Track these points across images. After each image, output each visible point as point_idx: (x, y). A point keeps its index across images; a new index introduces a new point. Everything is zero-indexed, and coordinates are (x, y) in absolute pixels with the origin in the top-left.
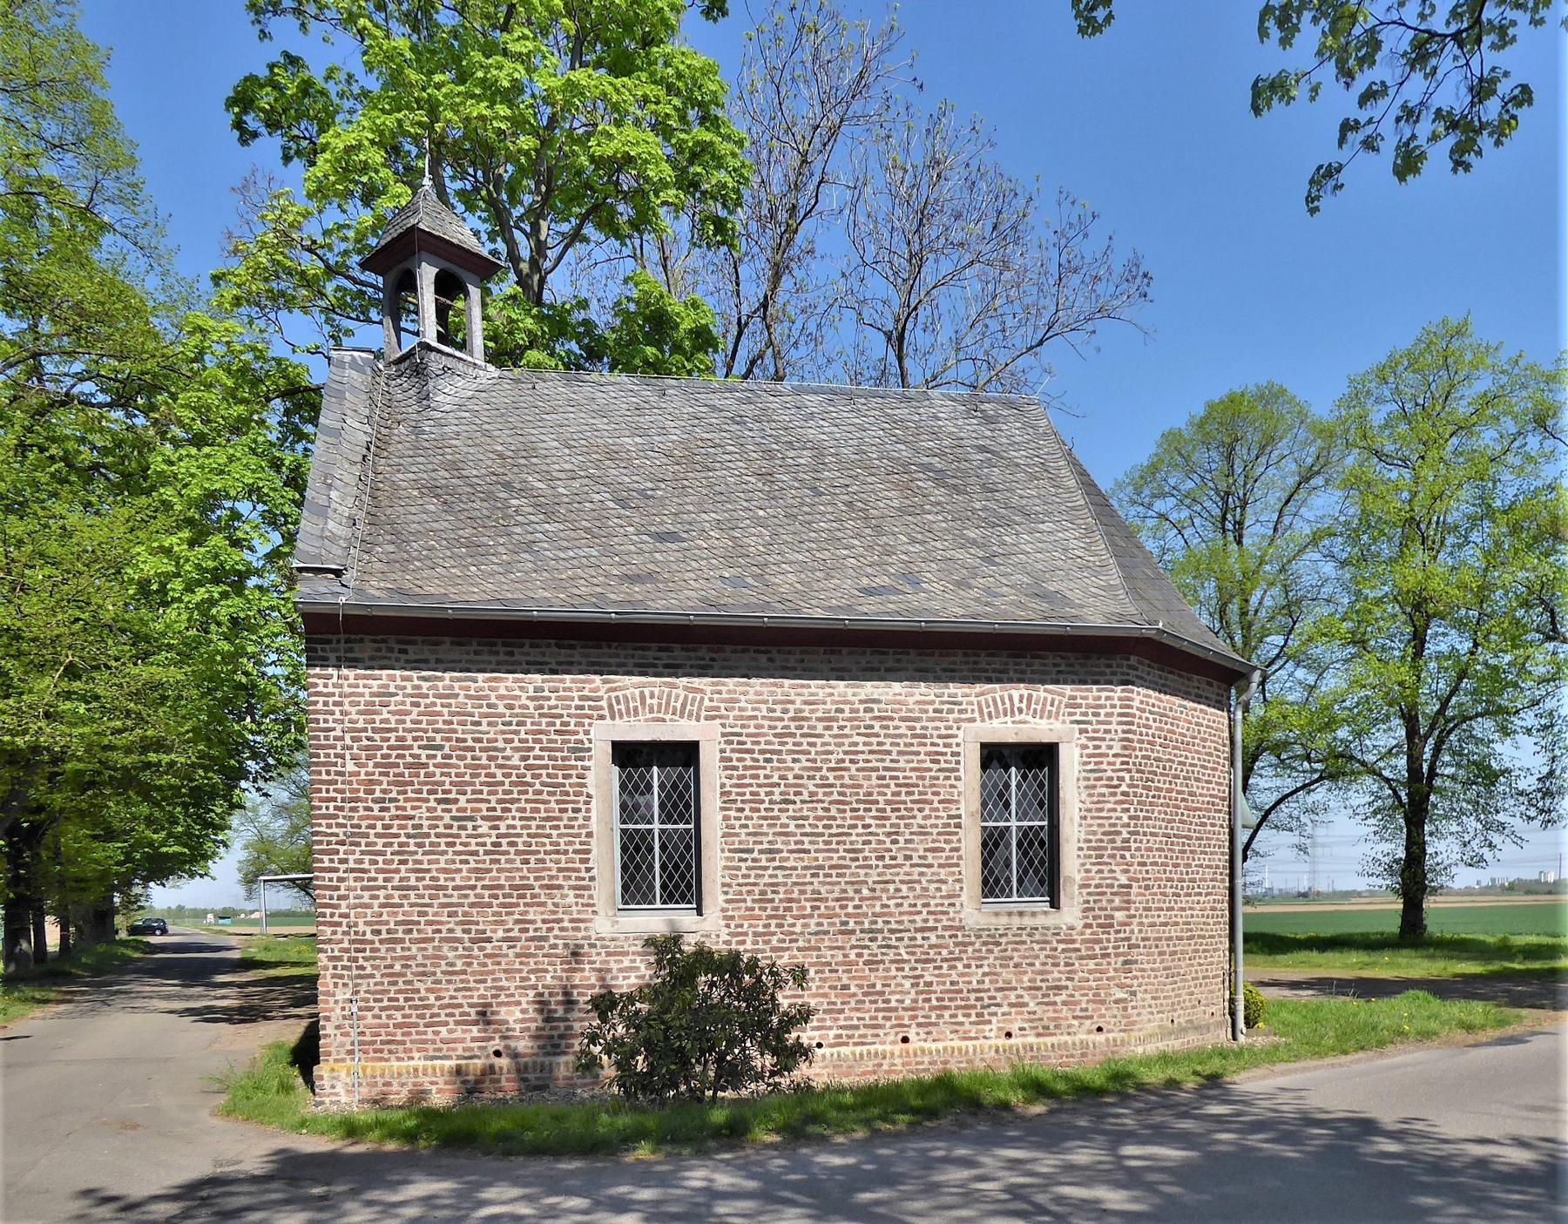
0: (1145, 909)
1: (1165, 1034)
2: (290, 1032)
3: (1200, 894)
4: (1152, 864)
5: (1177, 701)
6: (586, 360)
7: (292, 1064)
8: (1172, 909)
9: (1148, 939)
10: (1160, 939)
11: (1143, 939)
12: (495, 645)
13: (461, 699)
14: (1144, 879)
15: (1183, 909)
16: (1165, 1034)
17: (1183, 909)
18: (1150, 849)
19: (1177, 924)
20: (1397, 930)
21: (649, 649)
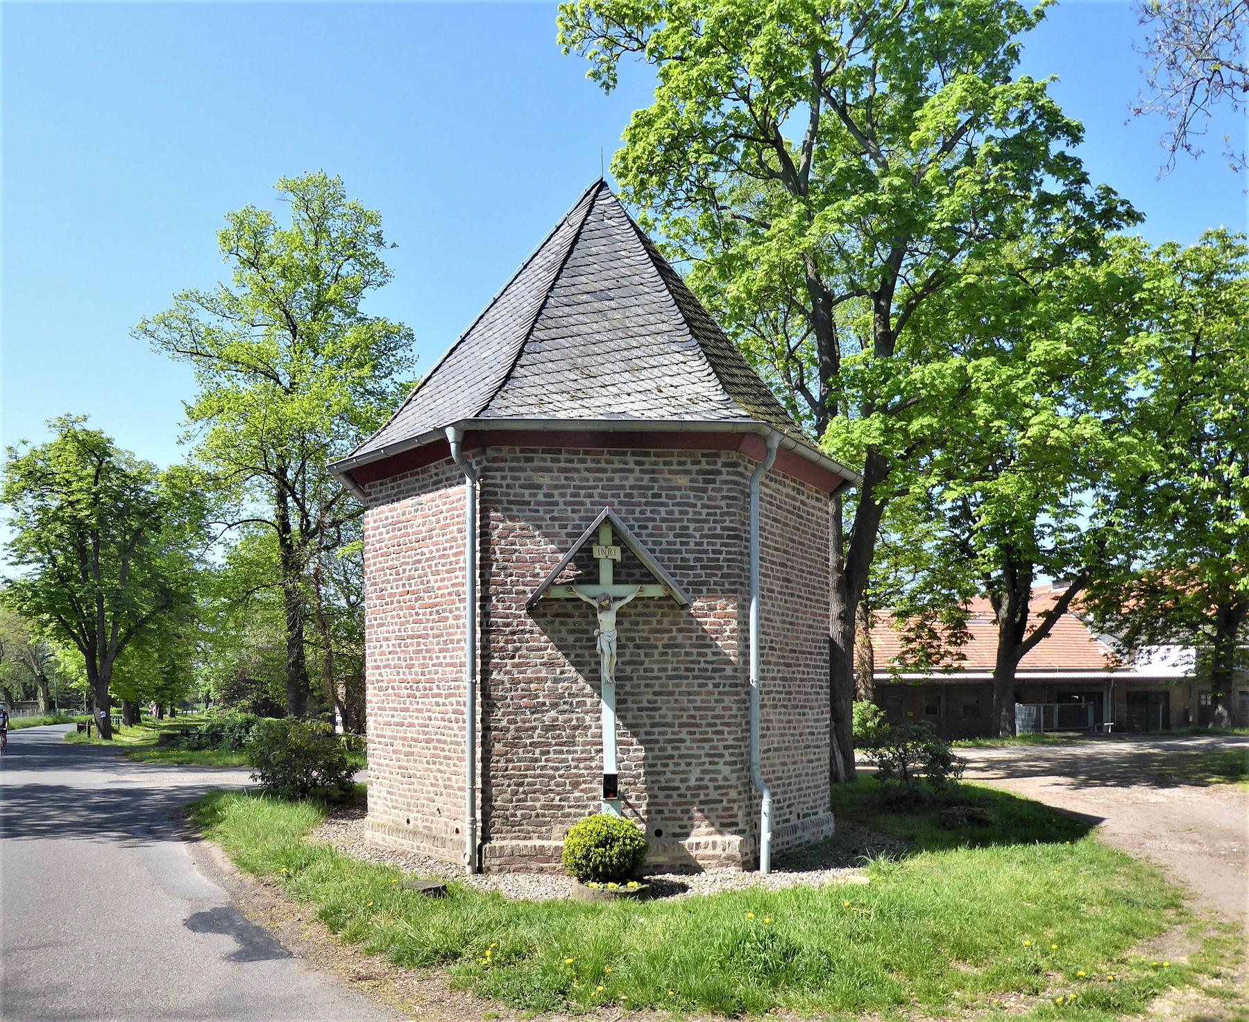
0: (380, 709)
1: (395, 830)
2: (283, 702)
3: (439, 695)
4: (385, 667)
5: (408, 502)
6: (998, 73)
7: (1049, 635)
8: (407, 710)
9: (382, 736)
10: (394, 738)
11: (378, 736)
12: (625, 454)
13: (562, 506)
14: (378, 681)
15: (419, 711)
16: (395, 830)
17: (419, 711)
18: (382, 653)
19: (411, 725)
20: (829, 828)
21: (602, 453)
